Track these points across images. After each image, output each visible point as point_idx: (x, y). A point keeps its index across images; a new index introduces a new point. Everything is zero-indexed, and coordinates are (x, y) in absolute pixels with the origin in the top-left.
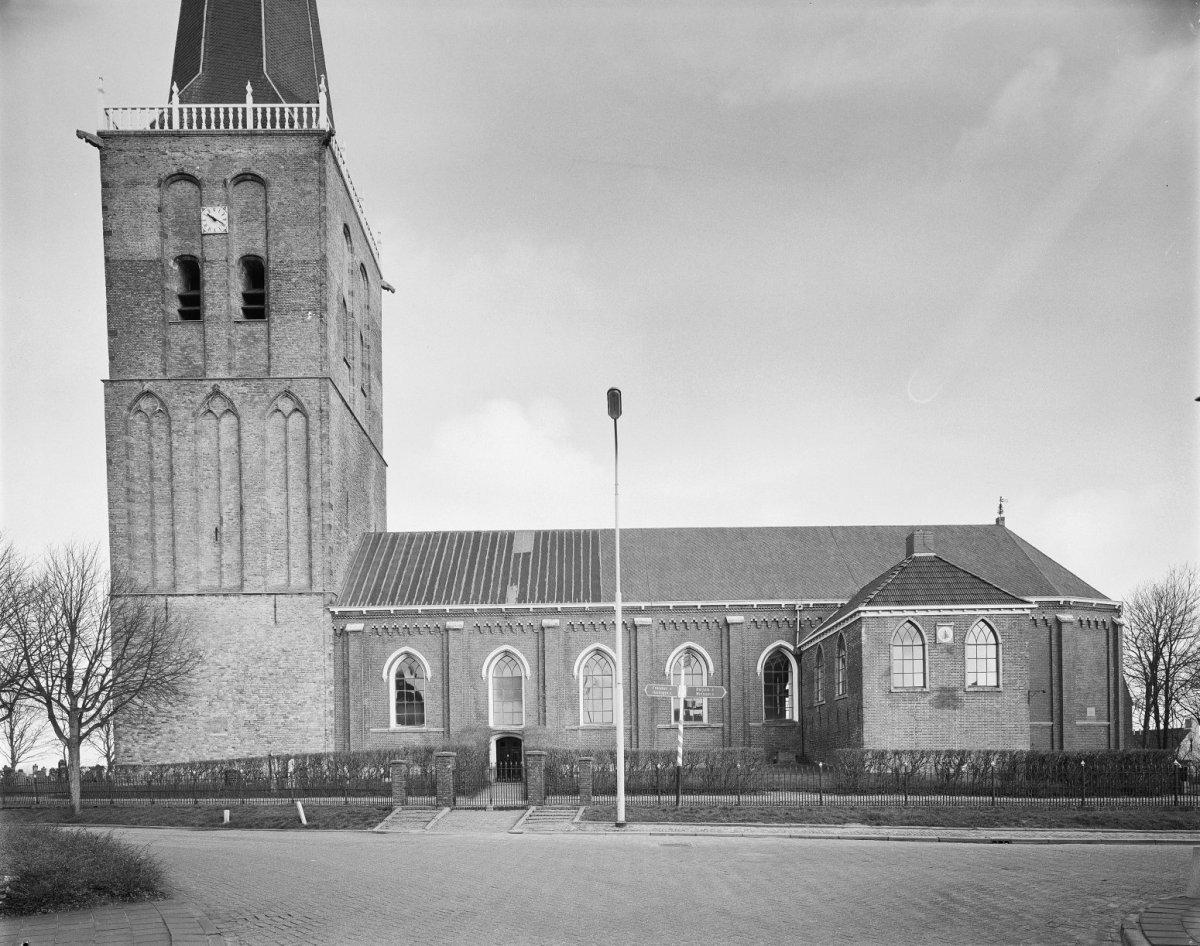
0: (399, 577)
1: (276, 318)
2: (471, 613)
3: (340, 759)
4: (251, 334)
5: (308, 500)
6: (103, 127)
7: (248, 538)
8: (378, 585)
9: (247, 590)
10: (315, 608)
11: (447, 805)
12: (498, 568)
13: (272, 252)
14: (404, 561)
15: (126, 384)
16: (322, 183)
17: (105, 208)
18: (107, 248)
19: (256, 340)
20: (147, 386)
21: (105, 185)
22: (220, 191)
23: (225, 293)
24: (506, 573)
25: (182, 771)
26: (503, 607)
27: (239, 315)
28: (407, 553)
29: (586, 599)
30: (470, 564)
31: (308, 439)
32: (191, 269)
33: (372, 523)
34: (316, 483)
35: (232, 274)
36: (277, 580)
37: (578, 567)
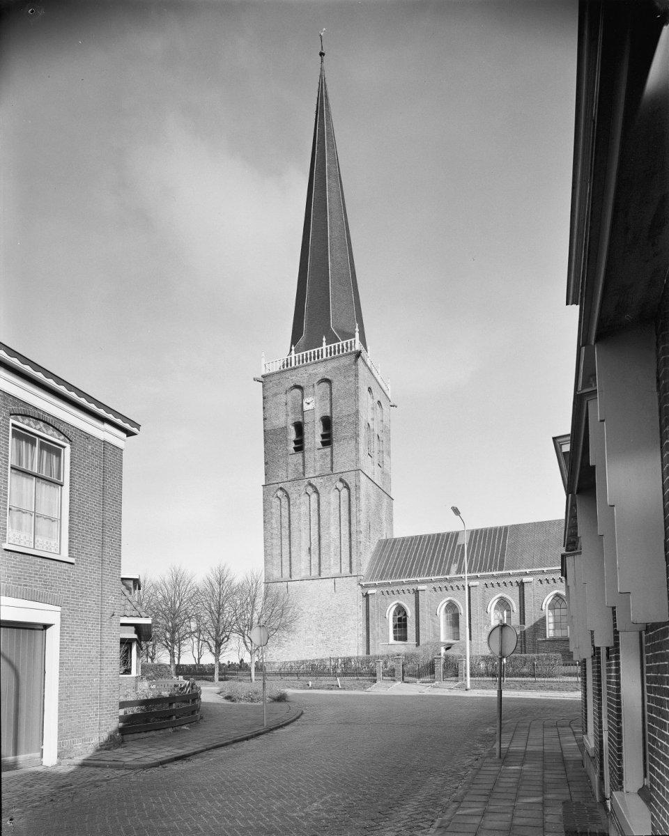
0: (395, 564)
1: (335, 444)
2: (431, 581)
3: (366, 661)
4: (325, 454)
5: (350, 530)
6: (264, 372)
7: (322, 551)
8: (384, 570)
9: (322, 576)
10: (353, 582)
11: (399, 680)
12: (448, 554)
13: (334, 412)
14: (399, 553)
15: (271, 486)
16: (356, 375)
17: (264, 408)
18: (264, 426)
19: (327, 456)
20: (280, 485)
21: (264, 398)
22: (311, 390)
23: (314, 434)
24: (452, 557)
25: (293, 665)
26: (448, 577)
27: (320, 445)
28: (400, 549)
29: (495, 569)
30: (432, 553)
31: (350, 500)
32: (299, 427)
33: (384, 533)
34: (353, 521)
35: (316, 427)
36: (335, 571)
37: (493, 550)
